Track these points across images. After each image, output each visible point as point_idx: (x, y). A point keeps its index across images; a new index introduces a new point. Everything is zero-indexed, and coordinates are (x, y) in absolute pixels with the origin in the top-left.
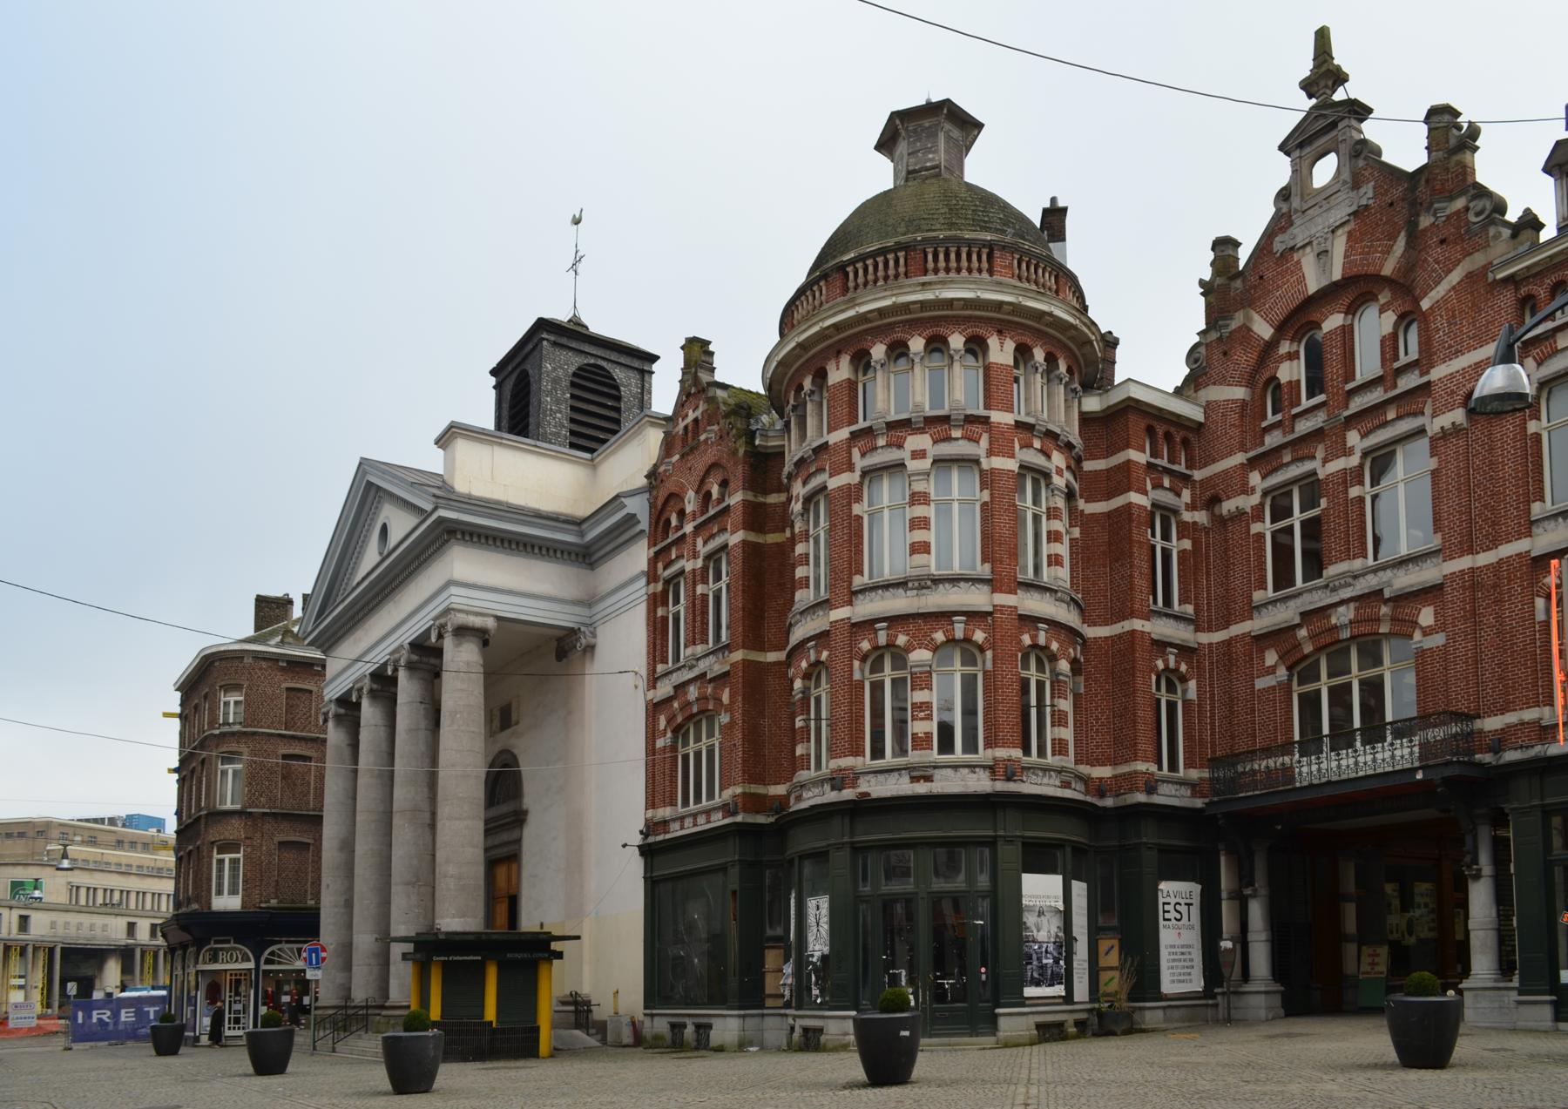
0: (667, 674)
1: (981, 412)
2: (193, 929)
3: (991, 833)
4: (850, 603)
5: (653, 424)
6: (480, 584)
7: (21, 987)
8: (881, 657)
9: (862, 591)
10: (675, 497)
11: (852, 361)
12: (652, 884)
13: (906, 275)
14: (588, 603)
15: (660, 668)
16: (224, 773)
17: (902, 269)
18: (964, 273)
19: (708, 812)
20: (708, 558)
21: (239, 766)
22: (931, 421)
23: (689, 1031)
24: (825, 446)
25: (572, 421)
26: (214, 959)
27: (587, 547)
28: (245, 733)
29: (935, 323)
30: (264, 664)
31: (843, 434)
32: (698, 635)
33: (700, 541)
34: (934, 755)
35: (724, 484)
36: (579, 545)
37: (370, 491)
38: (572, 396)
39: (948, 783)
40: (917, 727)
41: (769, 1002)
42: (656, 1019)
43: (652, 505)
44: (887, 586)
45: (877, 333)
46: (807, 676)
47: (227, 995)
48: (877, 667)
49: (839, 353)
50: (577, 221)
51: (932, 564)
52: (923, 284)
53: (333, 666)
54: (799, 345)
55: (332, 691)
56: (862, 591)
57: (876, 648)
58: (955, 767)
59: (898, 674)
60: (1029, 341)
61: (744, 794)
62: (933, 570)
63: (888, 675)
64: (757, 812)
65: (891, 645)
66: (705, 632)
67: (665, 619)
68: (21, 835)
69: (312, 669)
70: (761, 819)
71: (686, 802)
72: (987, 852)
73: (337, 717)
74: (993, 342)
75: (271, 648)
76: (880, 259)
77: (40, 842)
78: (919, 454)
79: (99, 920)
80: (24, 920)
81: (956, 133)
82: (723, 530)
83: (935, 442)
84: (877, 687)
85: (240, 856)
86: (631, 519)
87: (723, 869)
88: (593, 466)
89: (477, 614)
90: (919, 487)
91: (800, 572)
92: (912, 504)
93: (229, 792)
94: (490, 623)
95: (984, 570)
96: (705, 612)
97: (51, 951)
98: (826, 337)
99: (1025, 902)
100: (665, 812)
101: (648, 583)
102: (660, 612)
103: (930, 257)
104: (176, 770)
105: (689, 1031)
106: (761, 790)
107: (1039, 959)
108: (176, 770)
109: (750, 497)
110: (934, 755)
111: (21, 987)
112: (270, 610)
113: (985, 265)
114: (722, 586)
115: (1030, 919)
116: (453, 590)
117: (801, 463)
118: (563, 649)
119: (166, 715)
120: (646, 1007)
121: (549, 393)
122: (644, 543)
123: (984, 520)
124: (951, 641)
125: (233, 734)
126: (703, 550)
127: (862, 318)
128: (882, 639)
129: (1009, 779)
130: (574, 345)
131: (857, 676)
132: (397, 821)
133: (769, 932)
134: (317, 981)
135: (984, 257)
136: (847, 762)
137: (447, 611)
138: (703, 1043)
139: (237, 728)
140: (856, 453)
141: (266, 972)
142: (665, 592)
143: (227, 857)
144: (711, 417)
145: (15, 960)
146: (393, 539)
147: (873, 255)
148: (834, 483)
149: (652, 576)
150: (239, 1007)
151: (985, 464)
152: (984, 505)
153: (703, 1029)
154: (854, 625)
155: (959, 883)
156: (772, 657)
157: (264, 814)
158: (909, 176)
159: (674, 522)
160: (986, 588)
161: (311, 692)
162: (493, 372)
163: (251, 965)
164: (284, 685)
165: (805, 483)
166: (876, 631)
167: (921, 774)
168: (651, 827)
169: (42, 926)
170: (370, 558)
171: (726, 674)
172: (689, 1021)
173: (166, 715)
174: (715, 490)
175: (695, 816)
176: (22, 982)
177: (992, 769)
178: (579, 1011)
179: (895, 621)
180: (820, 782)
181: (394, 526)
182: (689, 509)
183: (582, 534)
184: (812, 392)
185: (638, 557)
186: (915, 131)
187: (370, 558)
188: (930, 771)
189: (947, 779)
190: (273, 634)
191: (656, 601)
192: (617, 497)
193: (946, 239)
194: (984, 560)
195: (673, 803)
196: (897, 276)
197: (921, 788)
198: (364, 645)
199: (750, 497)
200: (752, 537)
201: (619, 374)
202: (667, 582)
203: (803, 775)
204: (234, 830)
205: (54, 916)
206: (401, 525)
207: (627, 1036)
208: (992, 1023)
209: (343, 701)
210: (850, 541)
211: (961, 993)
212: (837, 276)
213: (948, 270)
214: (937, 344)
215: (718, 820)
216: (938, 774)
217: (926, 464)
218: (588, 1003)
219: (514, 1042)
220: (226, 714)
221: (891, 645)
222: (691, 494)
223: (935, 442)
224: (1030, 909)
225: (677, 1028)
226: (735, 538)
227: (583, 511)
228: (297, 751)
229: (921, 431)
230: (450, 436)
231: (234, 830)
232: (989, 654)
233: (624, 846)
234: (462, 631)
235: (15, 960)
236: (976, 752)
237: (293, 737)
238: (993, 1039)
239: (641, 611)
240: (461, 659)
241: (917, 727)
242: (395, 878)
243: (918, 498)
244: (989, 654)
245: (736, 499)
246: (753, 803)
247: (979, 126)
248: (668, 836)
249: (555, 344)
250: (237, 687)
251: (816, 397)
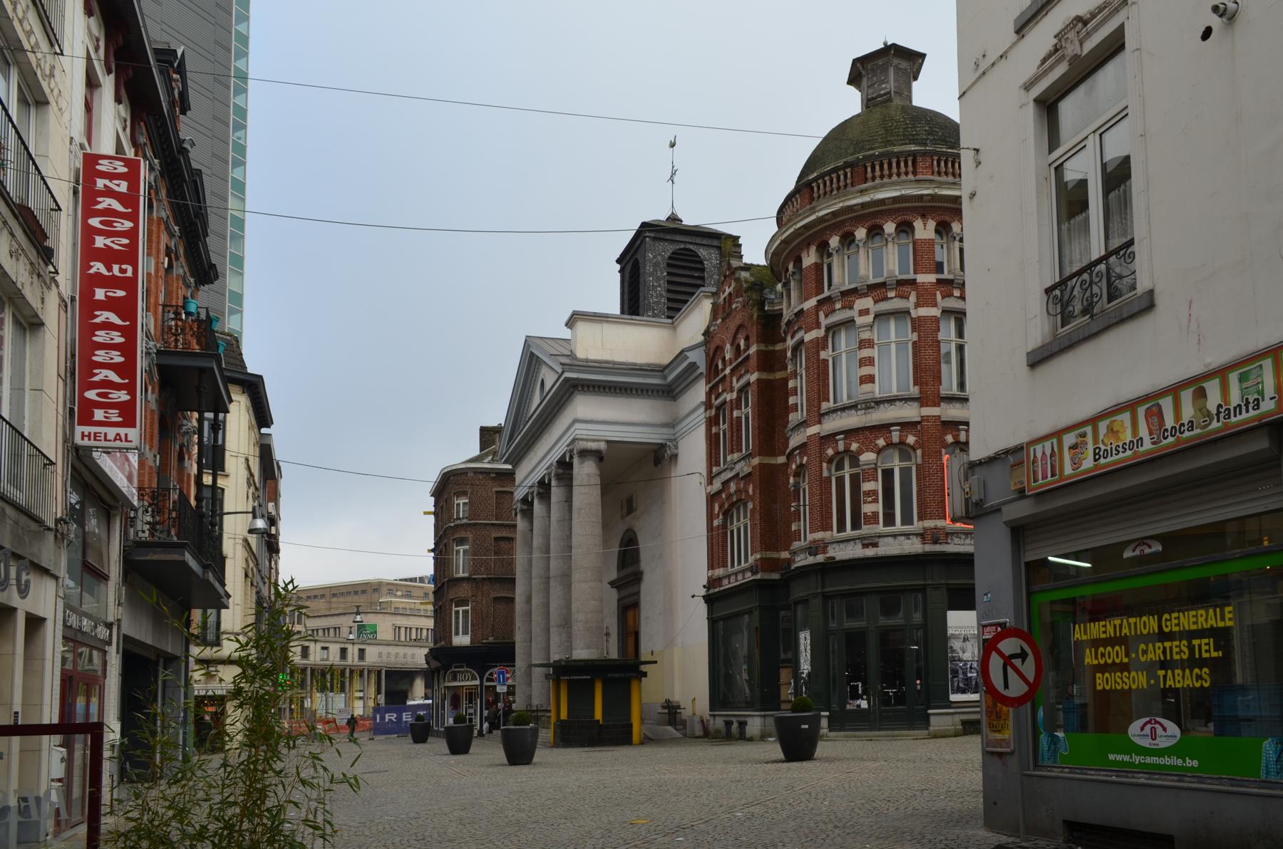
0: (720, 473)
1: (911, 276)
2: (444, 659)
3: (922, 582)
4: (820, 422)
5: (707, 297)
6: (598, 420)
7: (361, 698)
8: (843, 459)
9: (827, 413)
10: (719, 349)
11: (817, 250)
12: (712, 622)
13: (852, 185)
14: (672, 425)
15: (715, 469)
16: (458, 552)
17: (849, 181)
18: (895, 178)
19: (743, 571)
20: (740, 391)
22: (872, 288)
23: (735, 726)
24: (801, 311)
25: (669, 291)
26: (455, 679)
27: (670, 385)
29: (872, 217)
31: (812, 302)
32: (736, 447)
33: (734, 380)
34: (880, 528)
35: (747, 339)
36: (661, 385)
37: (531, 362)
38: (669, 274)
39: (889, 548)
40: (867, 509)
41: (783, 706)
43: (707, 354)
44: (843, 409)
45: (833, 228)
46: (797, 475)
47: (464, 703)
48: (840, 467)
49: (809, 245)
50: (673, 145)
51: (876, 390)
52: (862, 191)
53: (519, 476)
54: (782, 242)
55: (519, 494)
56: (827, 413)
57: (837, 453)
58: (895, 536)
59: (855, 470)
60: (947, 219)
61: (762, 559)
62: (877, 395)
63: (847, 472)
64: (772, 571)
65: (847, 451)
66: (740, 444)
67: (717, 435)
68: (364, 592)
69: (509, 476)
70: (776, 576)
71: (733, 566)
72: (920, 596)
73: (522, 511)
74: (918, 224)
75: (485, 465)
76: (834, 176)
77: (376, 595)
78: (864, 312)
79: (409, 651)
80: (362, 651)
81: (904, 64)
82: (747, 372)
83: (876, 302)
84: (840, 481)
86: (693, 366)
87: (750, 612)
88: (673, 327)
89: (594, 441)
90: (865, 335)
91: (792, 400)
92: (860, 348)
93: (461, 567)
94: (603, 446)
95: (914, 391)
96: (739, 430)
97: (379, 673)
98: (800, 235)
99: (950, 632)
100: (719, 572)
102: (714, 430)
103: (869, 169)
104: (432, 551)
105: (735, 726)
106: (774, 555)
107: (965, 674)
108: (432, 551)
109: (763, 347)
110: (880, 528)
111: (361, 698)
112: (488, 435)
113: (910, 169)
114: (747, 412)
115: (956, 645)
116: (577, 426)
117: (789, 323)
118: (657, 458)
119: (425, 513)
121: (651, 274)
123: (915, 354)
124: (890, 445)
125: (462, 525)
126: (736, 385)
127: (821, 220)
128: (841, 447)
129: (935, 542)
130: (668, 237)
131: (825, 474)
132: (552, 583)
133: (783, 656)
135: (910, 163)
136: (820, 535)
137: (574, 440)
138: (742, 737)
139: (465, 521)
140: (821, 314)
142: (717, 416)
143: (461, 609)
144: (738, 292)
145: (356, 678)
146: (548, 386)
147: (829, 173)
148: (809, 337)
149: (708, 405)
150: (471, 711)
151: (914, 315)
152: (914, 343)
153: (742, 725)
154: (822, 438)
155: (898, 620)
156: (781, 460)
158: (868, 103)
159: (720, 367)
160: (916, 404)
162: (618, 261)
163: (477, 682)
165: (792, 337)
166: (837, 441)
167: (870, 542)
168: (712, 582)
169: (374, 656)
171: (750, 474)
172: (734, 720)
173: (425, 513)
174: (742, 343)
175: (736, 574)
176: (361, 694)
177: (922, 535)
178: (672, 712)
179: (850, 433)
180: (803, 550)
181: (550, 381)
182: (728, 357)
183: (665, 378)
184: (794, 273)
185: (699, 392)
186: (872, 70)
188: (876, 540)
189: (888, 544)
190: (487, 455)
191: (712, 422)
192: (682, 351)
193: (882, 155)
194: (915, 384)
195: (725, 565)
196: (846, 186)
197: (870, 552)
198: (534, 462)
199: (763, 347)
200: (765, 376)
201: (702, 252)
202: (718, 408)
203: (796, 545)
204: (464, 591)
205: (381, 649)
206: (549, 378)
207: (698, 731)
208: (925, 721)
209: (525, 500)
210: (820, 376)
211: (900, 699)
212: (806, 190)
213: (882, 177)
214: (875, 231)
215: (749, 577)
216: (882, 541)
217: (869, 319)
218: (679, 707)
219: (615, 734)
220: (458, 512)
221: (847, 451)
222: (728, 346)
223: (876, 302)
224: (955, 637)
225: (728, 724)
226: (753, 377)
227: (666, 361)
228: (504, 534)
229: (865, 295)
230: (574, 319)
232: (919, 452)
234: (584, 453)
235: (356, 678)
236: (912, 524)
238: (926, 732)
240: (585, 471)
241: (867, 509)
242: (552, 623)
243: (867, 344)
244: (919, 452)
245: (753, 350)
246: (767, 564)
247: (923, 56)
249: (654, 239)
250: (464, 494)
251: (797, 277)
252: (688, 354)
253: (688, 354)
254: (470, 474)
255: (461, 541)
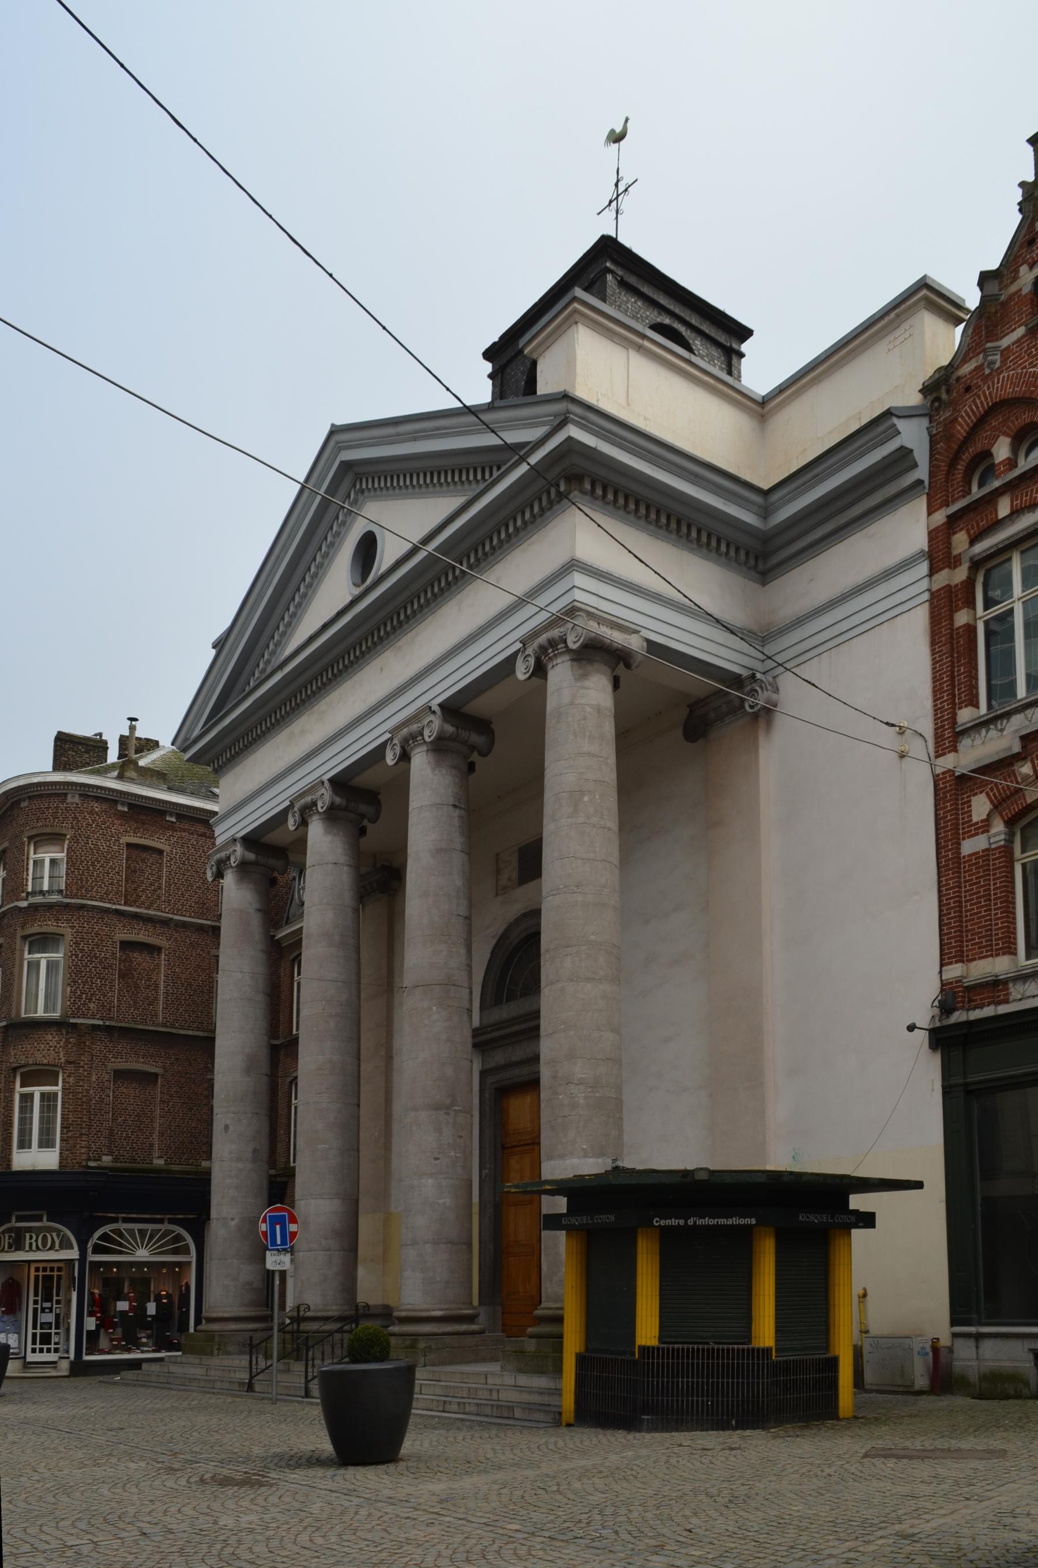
14: (760, 636)
16: (34, 966)
21: (58, 956)
28: (67, 906)
30: (97, 807)
42: (987, 1345)
50: (616, 138)
73: (244, 867)
85: (58, 1089)
86: (904, 455)
94: (634, 643)
101: (932, 573)
116: (578, 579)
120: (953, 1323)
122: (921, 504)
125: (50, 907)
130: (645, 289)
134: (283, 1274)
139: (55, 898)
141: (96, 1265)
143: (37, 1091)
149: (938, 554)
150: (50, 1318)
157: (95, 1027)
161: (160, 852)
163: (74, 1254)
164: (125, 840)
168: (951, 997)
170: (335, 591)
185: (909, 528)
187: (335, 591)
191: (943, 605)
192: (888, 414)
202: (976, 565)
204: (49, 1049)
228: (142, 937)
231: (49, 1049)
233: (911, 1028)
234: (595, 652)
237: (136, 916)
239: (919, 619)
240: (581, 710)
248: (1003, 1009)
249: (623, 284)
250: (55, 838)
252: (901, 424)
253: (901, 424)
254: (73, 799)
255: (43, 942)
